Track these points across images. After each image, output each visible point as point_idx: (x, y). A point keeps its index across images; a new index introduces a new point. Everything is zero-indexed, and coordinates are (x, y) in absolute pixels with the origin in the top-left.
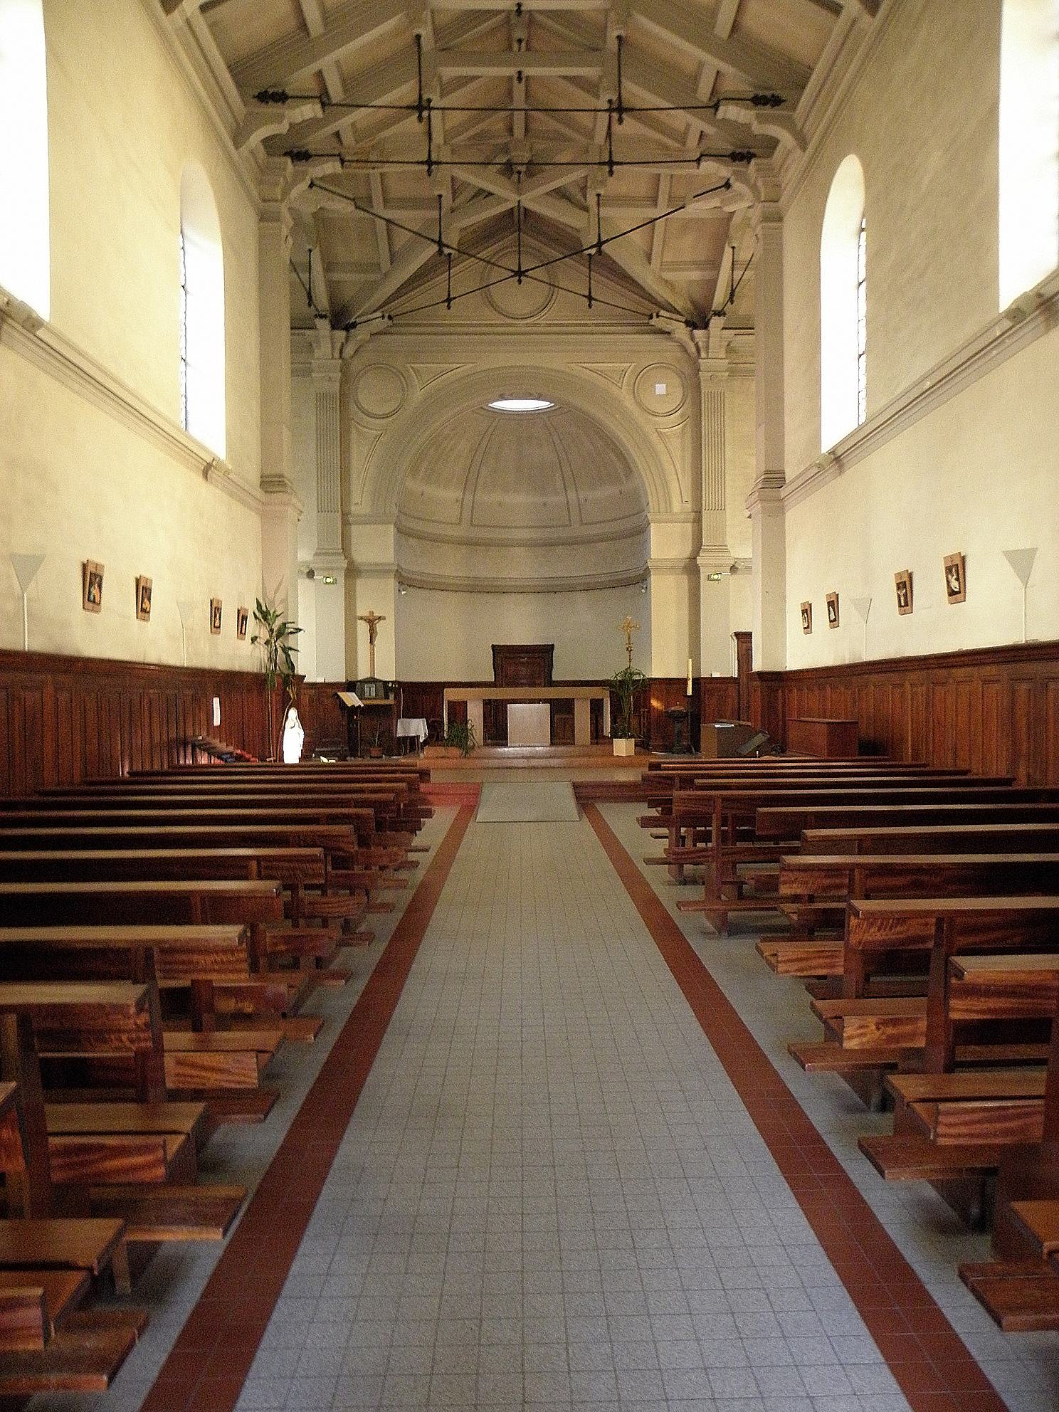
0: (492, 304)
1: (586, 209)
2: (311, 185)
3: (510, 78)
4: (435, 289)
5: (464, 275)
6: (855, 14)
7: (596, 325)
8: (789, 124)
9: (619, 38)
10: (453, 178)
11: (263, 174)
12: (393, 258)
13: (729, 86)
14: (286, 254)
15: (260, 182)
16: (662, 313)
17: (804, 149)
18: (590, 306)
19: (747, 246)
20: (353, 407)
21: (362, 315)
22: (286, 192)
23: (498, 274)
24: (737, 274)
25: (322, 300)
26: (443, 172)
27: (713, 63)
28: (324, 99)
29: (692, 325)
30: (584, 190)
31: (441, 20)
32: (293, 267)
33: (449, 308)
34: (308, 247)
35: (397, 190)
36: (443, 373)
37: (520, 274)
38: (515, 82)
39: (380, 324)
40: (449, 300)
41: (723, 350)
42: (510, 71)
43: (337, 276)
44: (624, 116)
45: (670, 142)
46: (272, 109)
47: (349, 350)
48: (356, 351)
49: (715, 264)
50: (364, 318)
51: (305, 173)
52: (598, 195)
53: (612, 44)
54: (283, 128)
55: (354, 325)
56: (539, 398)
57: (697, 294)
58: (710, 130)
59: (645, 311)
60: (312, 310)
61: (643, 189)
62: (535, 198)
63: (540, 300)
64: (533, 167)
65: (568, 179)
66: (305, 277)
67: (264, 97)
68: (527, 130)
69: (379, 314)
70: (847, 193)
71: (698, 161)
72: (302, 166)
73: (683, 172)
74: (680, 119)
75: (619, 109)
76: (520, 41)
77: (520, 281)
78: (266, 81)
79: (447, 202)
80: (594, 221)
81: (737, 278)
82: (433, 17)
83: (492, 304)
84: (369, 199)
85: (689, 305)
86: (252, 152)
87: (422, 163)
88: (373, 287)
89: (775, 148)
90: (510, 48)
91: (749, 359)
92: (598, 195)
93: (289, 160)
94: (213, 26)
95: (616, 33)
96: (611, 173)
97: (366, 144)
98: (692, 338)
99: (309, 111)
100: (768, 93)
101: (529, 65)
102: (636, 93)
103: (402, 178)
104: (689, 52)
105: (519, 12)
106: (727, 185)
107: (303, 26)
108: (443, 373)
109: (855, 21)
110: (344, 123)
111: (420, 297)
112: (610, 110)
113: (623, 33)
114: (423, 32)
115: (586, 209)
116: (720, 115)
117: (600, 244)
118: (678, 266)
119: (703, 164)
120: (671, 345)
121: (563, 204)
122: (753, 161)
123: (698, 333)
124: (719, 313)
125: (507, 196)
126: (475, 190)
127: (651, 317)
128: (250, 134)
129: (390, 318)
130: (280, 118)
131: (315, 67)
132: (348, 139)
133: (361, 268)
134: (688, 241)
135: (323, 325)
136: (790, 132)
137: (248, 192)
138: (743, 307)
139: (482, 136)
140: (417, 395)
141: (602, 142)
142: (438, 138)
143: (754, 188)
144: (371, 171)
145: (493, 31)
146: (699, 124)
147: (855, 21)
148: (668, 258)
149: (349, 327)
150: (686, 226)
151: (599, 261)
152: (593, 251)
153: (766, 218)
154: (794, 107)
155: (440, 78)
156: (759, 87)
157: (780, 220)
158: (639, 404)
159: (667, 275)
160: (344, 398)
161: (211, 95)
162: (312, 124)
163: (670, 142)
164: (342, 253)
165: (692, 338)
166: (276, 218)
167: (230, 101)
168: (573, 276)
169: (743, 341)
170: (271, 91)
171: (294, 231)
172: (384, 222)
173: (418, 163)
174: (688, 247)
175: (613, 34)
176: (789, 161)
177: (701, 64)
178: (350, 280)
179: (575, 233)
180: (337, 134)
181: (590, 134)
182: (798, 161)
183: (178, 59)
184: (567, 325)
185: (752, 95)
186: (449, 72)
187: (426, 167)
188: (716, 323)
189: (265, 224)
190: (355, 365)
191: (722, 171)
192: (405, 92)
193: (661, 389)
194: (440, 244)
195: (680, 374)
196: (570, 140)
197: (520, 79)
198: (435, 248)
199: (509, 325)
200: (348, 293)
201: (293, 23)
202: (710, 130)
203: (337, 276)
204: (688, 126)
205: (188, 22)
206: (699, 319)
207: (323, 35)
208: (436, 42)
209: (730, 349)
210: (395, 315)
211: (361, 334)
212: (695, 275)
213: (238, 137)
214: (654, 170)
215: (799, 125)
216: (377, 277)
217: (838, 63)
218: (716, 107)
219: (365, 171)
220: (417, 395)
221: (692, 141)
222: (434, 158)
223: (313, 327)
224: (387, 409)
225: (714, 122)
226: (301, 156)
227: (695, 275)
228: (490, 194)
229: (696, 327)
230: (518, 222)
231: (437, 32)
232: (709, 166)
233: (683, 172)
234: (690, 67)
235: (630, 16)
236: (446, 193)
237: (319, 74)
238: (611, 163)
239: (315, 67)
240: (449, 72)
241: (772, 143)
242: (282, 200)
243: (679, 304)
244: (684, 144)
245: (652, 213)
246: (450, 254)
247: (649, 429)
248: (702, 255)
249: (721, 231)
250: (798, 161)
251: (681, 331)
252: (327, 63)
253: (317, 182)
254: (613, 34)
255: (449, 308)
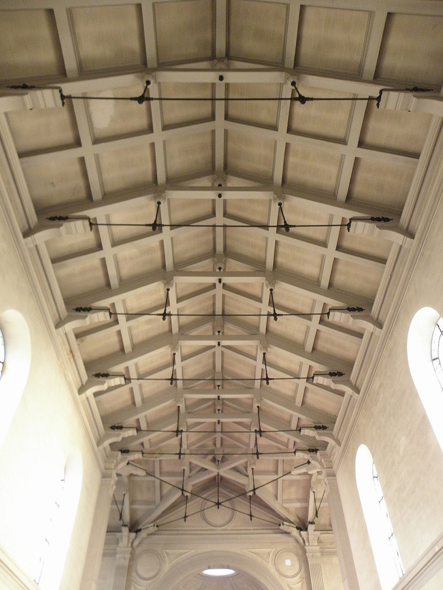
0: (205, 519)
1: (247, 476)
2: (128, 464)
3: (215, 423)
4: (180, 512)
5: (193, 505)
6: (351, 394)
7: (254, 530)
8: (331, 436)
9: (258, 407)
10: (190, 463)
11: (108, 458)
12: (161, 498)
13: (302, 423)
14: (111, 492)
15: (106, 462)
16: (285, 523)
17: (340, 445)
18: (251, 519)
19: (320, 490)
20: (134, 574)
21: (145, 525)
22: (116, 466)
23: (210, 504)
24: (318, 504)
25: (127, 517)
26: (187, 459)
27: (296, 415)
28: (138, 429)
29: (299, 529)
30: (246, 468)
31: (188, 403)
32: (115, 502)
33: (185, 520)
34: (124, 493)
35: (166, 468)
36: (181, 554)
37: (218, 504)
38: (217, 424)
39: (152, 529)
40: (185, 517)
41: (316, 541)
42: (216, 420)
43: (135, 507)
44: (269, 381)
45: (282, 447)
46: (117, 432)
47: (136, 543)
48: (140, 544)
49: (306, 500)
50: (145, 527)
51: (126, 458)
52: (253, 469)
53: (255, 410)
54: (119, 439)
55: (140, 530)
56: (228, 567)
57: (300, 514)
58: (298, 441)
59: (277, 522)
60: (121, 523)
61: (271, 467)
62: (225, 472)
63: (228, 518)
64: (223, 460)
65: (239, 463)
66: (120, 507)
67: (113, 428)
68: (222, 444)
69: (152, 524)
70: (363, 456)
71: (295, 452)
72: (125, 455)
73: (288, 458)
74: (284, 436)
75: (260, 432)
76: (219, 410)
77: (218, 508)
78: (116, 423)
79: (187, 473)
80: (251, 481)
81: (317, 506)
82: (185, 402)
83: (205, 519)
84: (154, 472)
85: (297, 520)
86: (104, 449)
87: (168, 379)
88: (149, 512)
89: (326, 447)
90: (214, 334)
91: (329, 546)
92: (253, 469)
93: (120, 453)
94: (98, 403)
95: (257, 405)
96: (258, 458)
97: (154, 448)
98: (301, 535)
99: (132, 432)
100: (321, 425)
101: (224, 418)
102: (265, 426)
103: (169, 461)
104: (286, 412)
105: (219, 398)
106: (309, 462)
107: (134, 403)
108: (181, 554)
109: (351, 396)
110: (145, 439)
111: (172, 516)
112: (262, 379)
113: (259, 405)
114: (180, 405)
115: (247, 476)
116: (315, 382)
117: (254, 490)
118: (290, 501)
119: (297, 453)
120: (291, 540)
121: (238, 474)
122: (318, 452)
123: (303, 533)
124: (312, 523)
125: (213, 470)
126: (199, 468)
127: (280, 525)
128: (104, 442)
129: (157, 526)
130: (118, 435)
131: (136, 417)
132: (147, 446)
133: (147, 503)
134: (293, 489)
135: (125, 530)
136: (350, 387)
137: (99, 464)
138: (322, 520)
139: (203, 446)
140: (167, 567)
141: (253, 448)
142: (184, 446)
143: (321, 463)
144: (155, 459)
145: (209, 407)
146: (293, 439)
147: (351, 396)
148: (285, 497)
149: (138, 531)
150: (291, 483)
151: (255, 500)
152: (251, 494)
153: (328, 475)
154: (332, 430)
155: (187, 424)
156: (316, 423)
157: (334, 475)
158: (278, 570)
159: (286, 505)
160: (130, 568)
161: (88, 417)
162: (132, 438)
163: (282, 447)
164: (139, 497)
165: (301, 535)
166: (110, 476)
167: (95, 417)
168: (242, 505)
169: (325, 537)
170: (117, 425)
171: (118, 483)
172: (156, 476)
173: (146, 225)
174: (294, 493)
175: (256, 405)
176: (334, 451)
177: (291, 416)
178: (140, 508)
179: (243, 487)
180: (142, 444)
181: (248, 445)
182: (338, 450)
183: (39, 298)
184: (241, 530)
185: (314, 426)
186: (191, 421)
187: (170, 381)
188: (311, 527)
189: (106, 479)
190: (138, 551)
191: (307, 456)
192: (173, 427)
193: (288, 562)
194: (183, 490)
195: (297, 555)
196: (240, 447)
197: (219, 423)
198: (181, 492)
199: (213, 530)
200: (139, 515)
201: (130, 403)
202: (298, 441)
203: (135, 507)
204: (289, 439)
205: (87, 398)
206: (302, 527)
207: (140, 407)
208: (183, 385)
209: (319, 541)
210: (159, 526)
211: (143, 534)
212: (298, 505)
213: (99, 443)
214: (275, 457)
215: (336, 437)
216: (152, 507)
217: (348, 411)
218: (300, 430)
219: (152, 459)
220: (167, 567)
221: (291, 446)
222: (182, 452)
223: (120, 531)
224: (151, 574)
225: (299, 437)
226: (125, 451)
227: (298, 505)
228: (206, 469)
229: (301, 530)
230: (218, 482)
231: (186, 407)
232: (299, 454)
233: (288, 458)
234: (286, 417)
235: (262, 399)
236: (187, 468)
237: (138, 421)
238: (258, 454)
239: (136, 417)
240: (191, 421)
241: (325, 445)
242: (115, 469)
243: (292, 519)
244: (288, 447)
245: (275, 477)
246: (187, 496)
247: (284, 585)
248: (300, 495)
249: (307, 486)
250: (338, 450)
251: (295, 532)
252: (141, 416)
253: (131, 462)
254: (256, 405)
255: (185, 520)
